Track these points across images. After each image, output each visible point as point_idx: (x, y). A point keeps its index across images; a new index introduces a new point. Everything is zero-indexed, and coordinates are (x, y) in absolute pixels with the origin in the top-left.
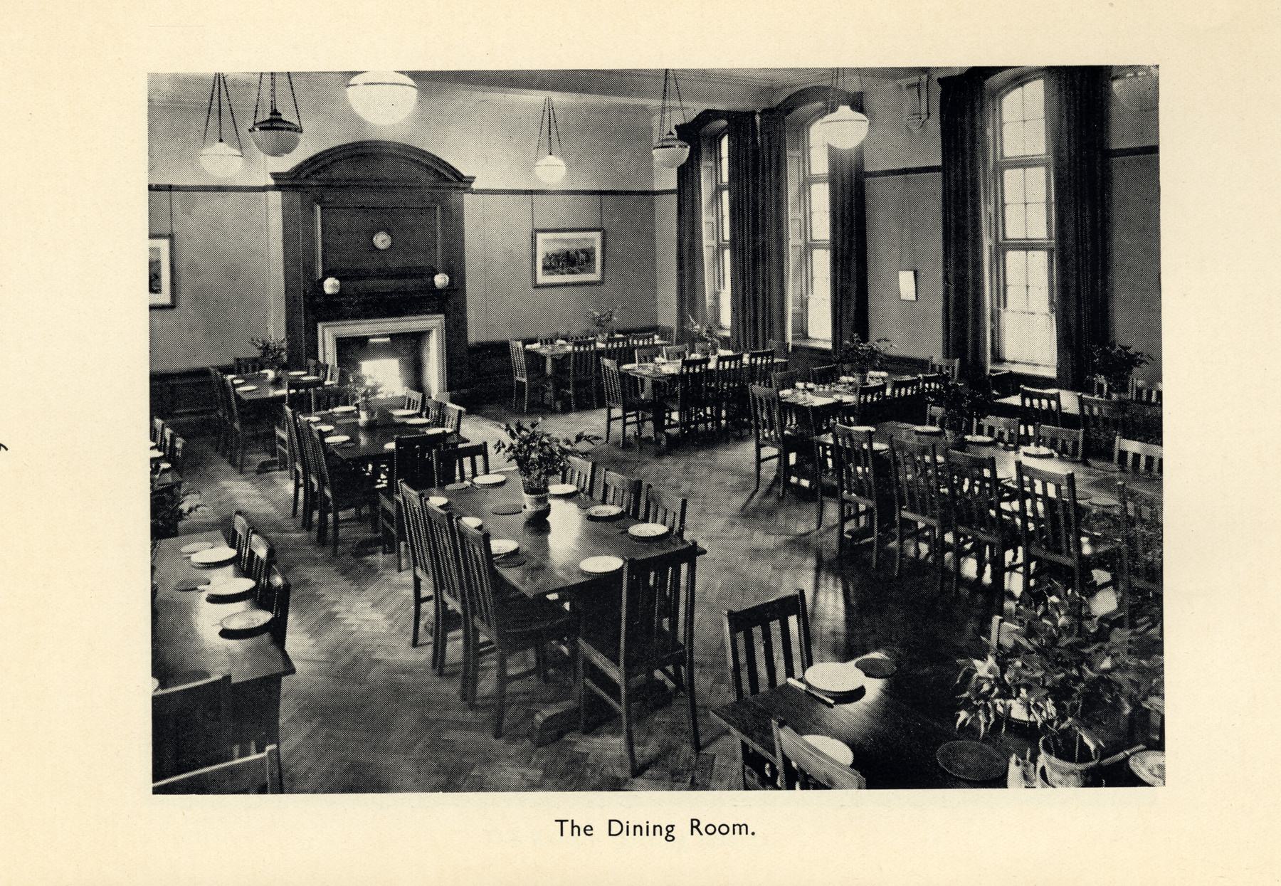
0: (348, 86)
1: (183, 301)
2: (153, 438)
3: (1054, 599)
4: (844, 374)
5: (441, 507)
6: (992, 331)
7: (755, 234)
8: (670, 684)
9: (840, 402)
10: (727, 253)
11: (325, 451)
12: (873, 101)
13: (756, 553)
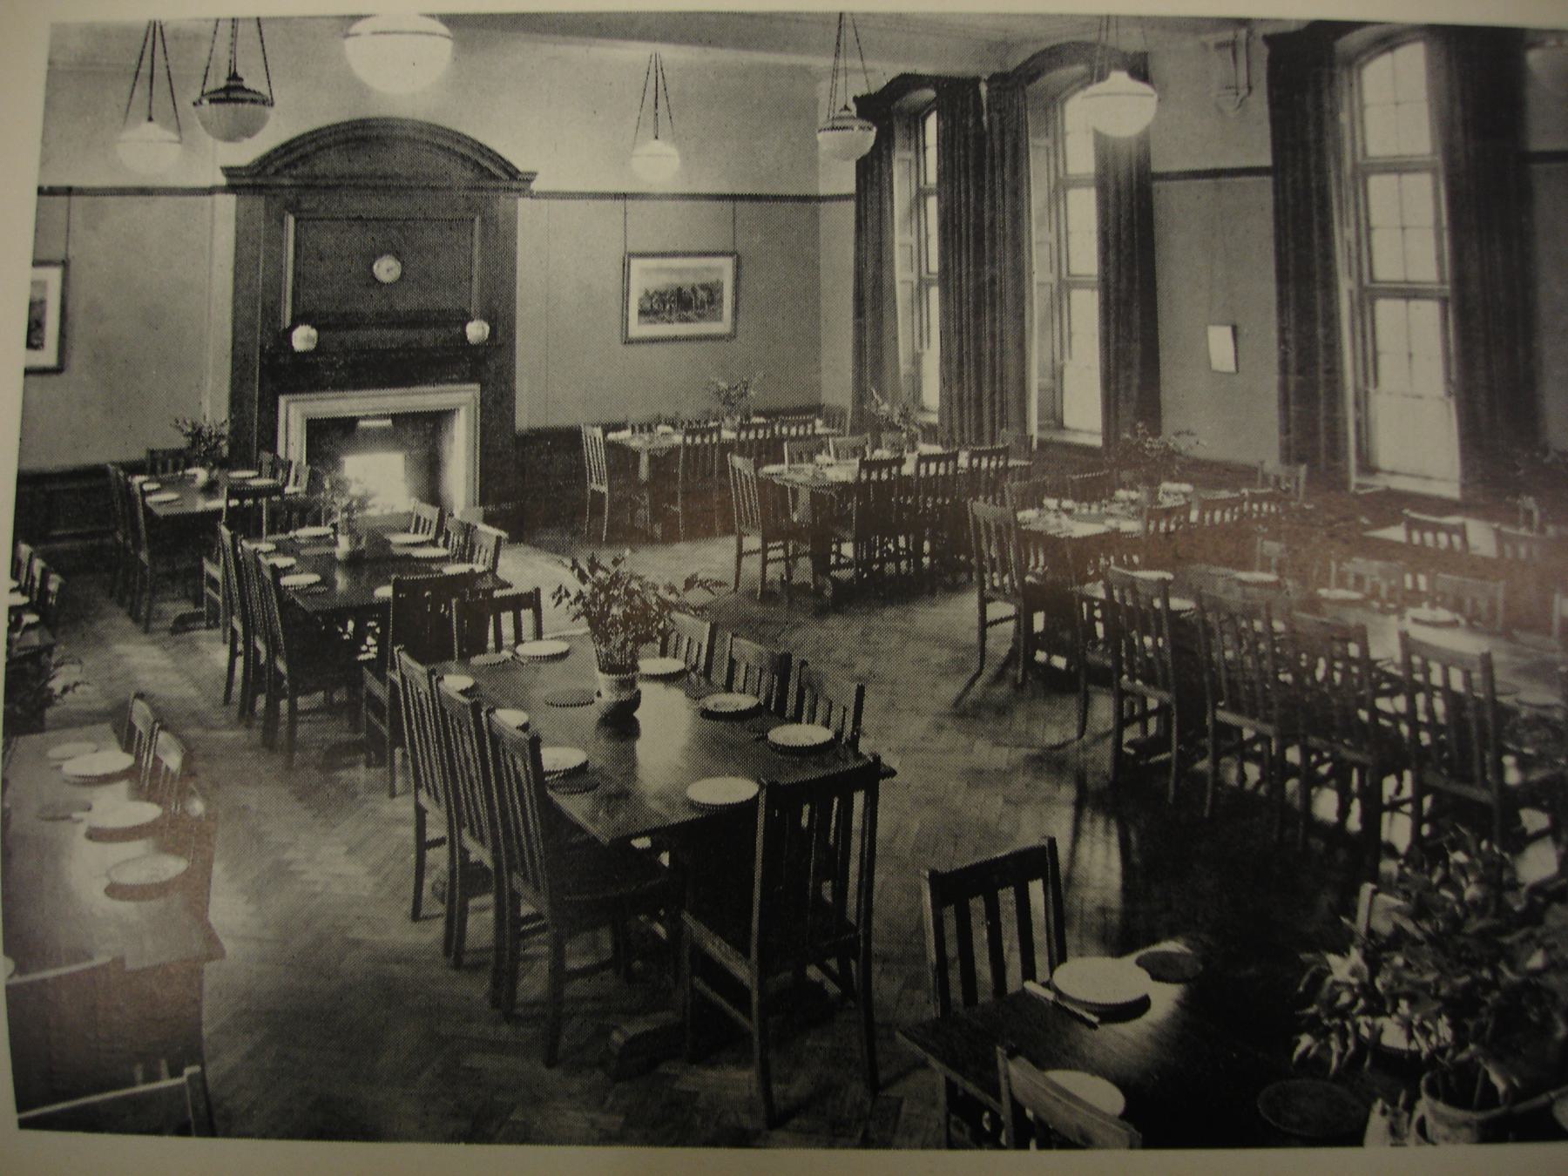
0: (347, 36)
1: (76, 361)
2: (15, 575)
3: (1460, 857)
4: (1123, 486)
5: (464, 692)
6: (1358, 424)
7: (979, 263)
8: (832, 988)
9: (1116, 531)
10: (935, 292)
11: (279, 599)
12: (1162, 66)
13: (977, 777)
